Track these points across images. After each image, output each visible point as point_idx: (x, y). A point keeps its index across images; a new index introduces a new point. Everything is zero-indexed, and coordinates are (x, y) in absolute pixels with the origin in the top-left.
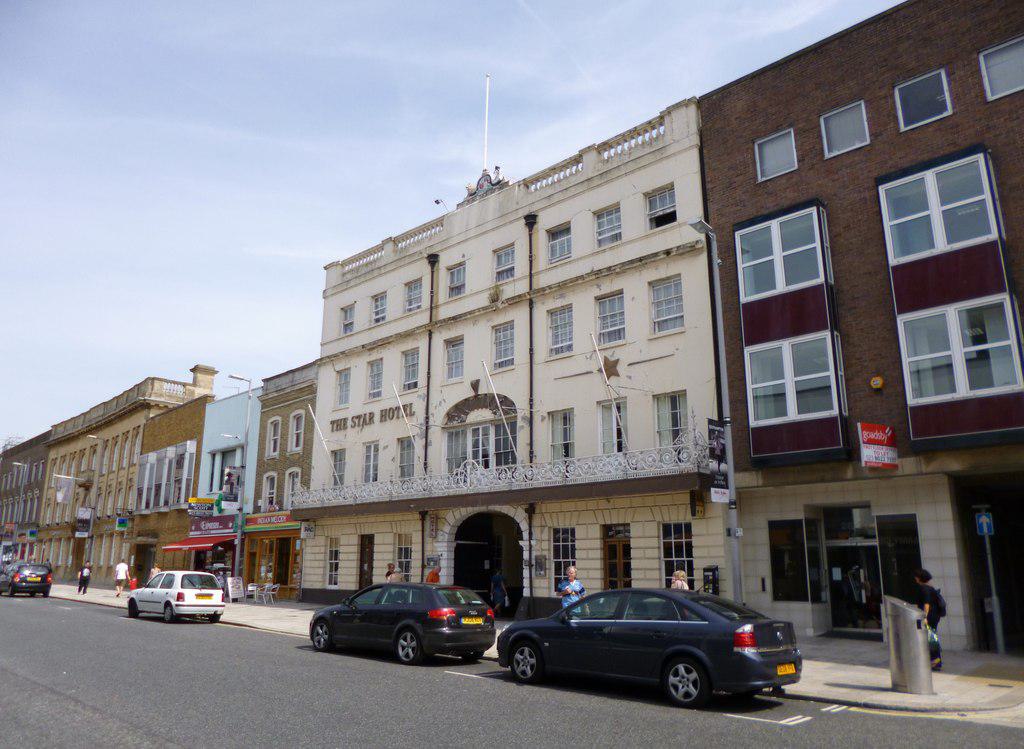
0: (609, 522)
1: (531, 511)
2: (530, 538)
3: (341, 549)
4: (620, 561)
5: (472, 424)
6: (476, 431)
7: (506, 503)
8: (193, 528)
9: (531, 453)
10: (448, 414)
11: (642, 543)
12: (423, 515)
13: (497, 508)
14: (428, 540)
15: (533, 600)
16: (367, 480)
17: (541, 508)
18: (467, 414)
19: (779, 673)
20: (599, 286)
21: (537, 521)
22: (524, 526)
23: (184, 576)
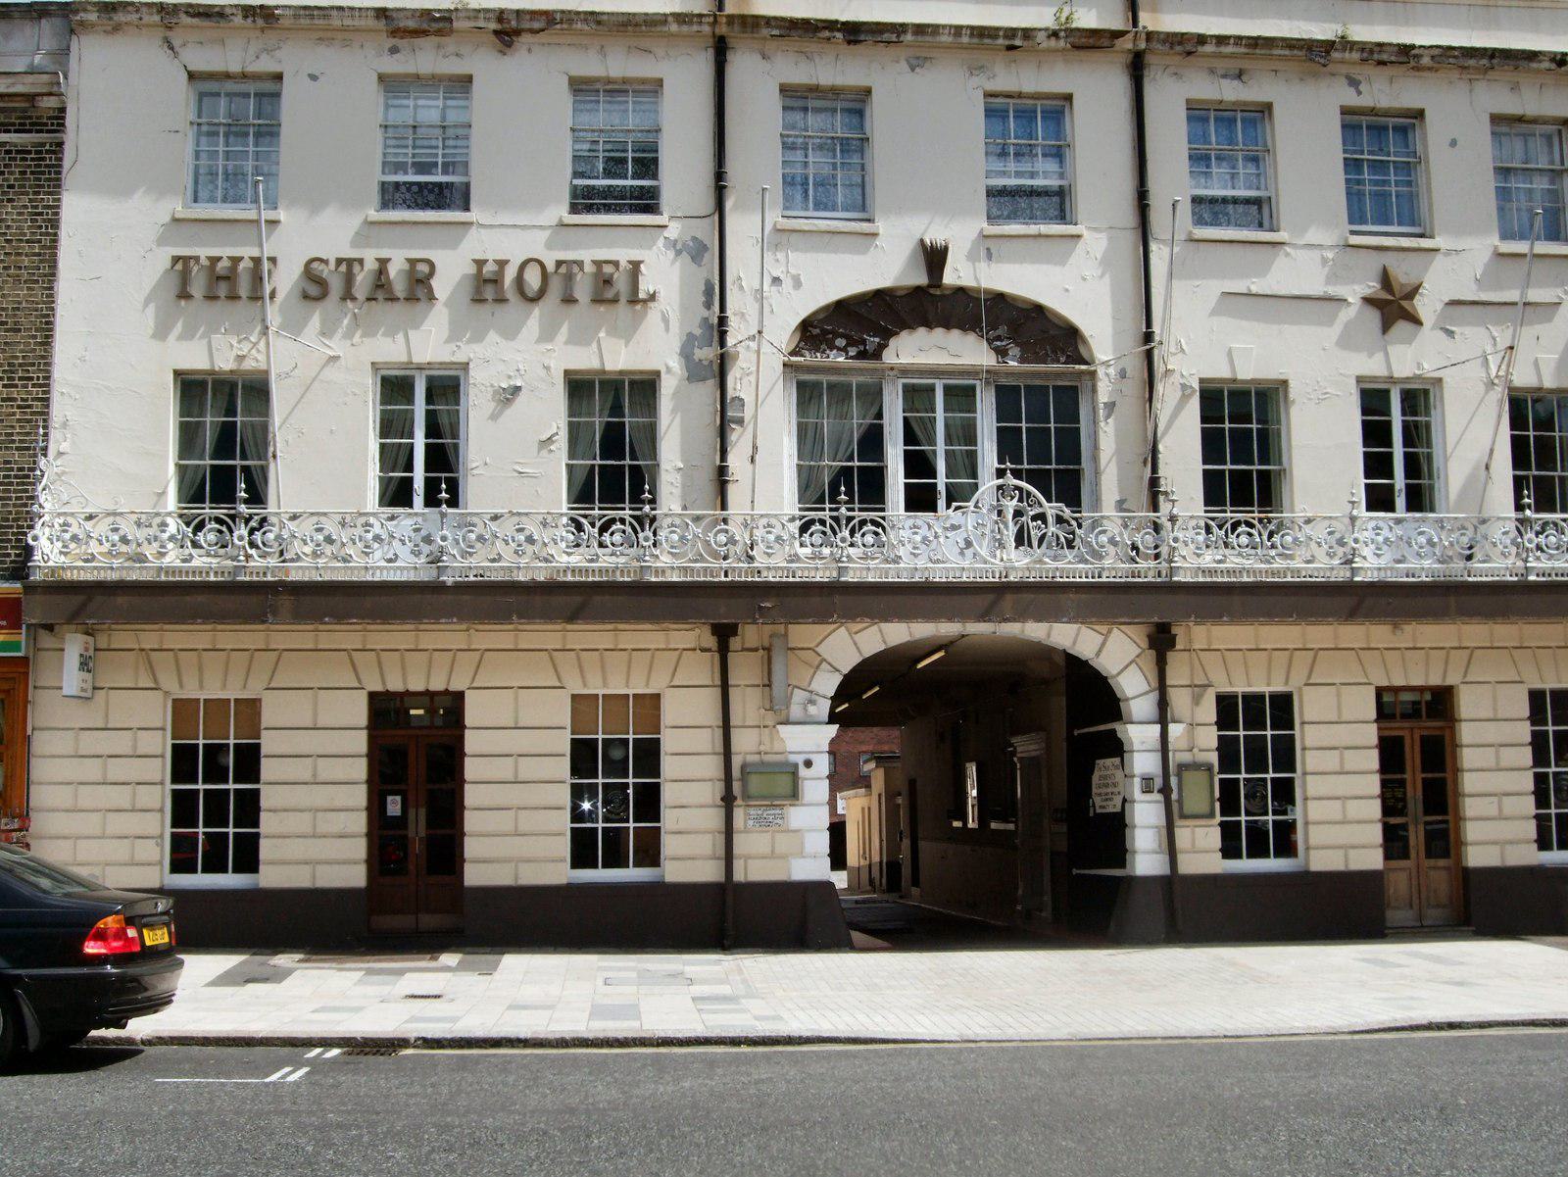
0: (395, 685)
1: (1161, 642)
2: (1163, 716)
3: (269, 743)
4: (1414, 777)
5: (905, 371)
6: (910, 392)
7: (1083, 616)
8: (957, 824)
9: (1154, 482)
10: (805, 326)
11: (1492, 732)
12: (724, 634)
13: (1035, 631)
14: (746, 705)
15: (1172, 884)
16: (397, 494)
17: (1195, 635)
18: (887, 335)
19: (390, 798)
20: (1354, 83)
21: (1176, 663)
22: (1133, 686)
23: (1061, 339)
